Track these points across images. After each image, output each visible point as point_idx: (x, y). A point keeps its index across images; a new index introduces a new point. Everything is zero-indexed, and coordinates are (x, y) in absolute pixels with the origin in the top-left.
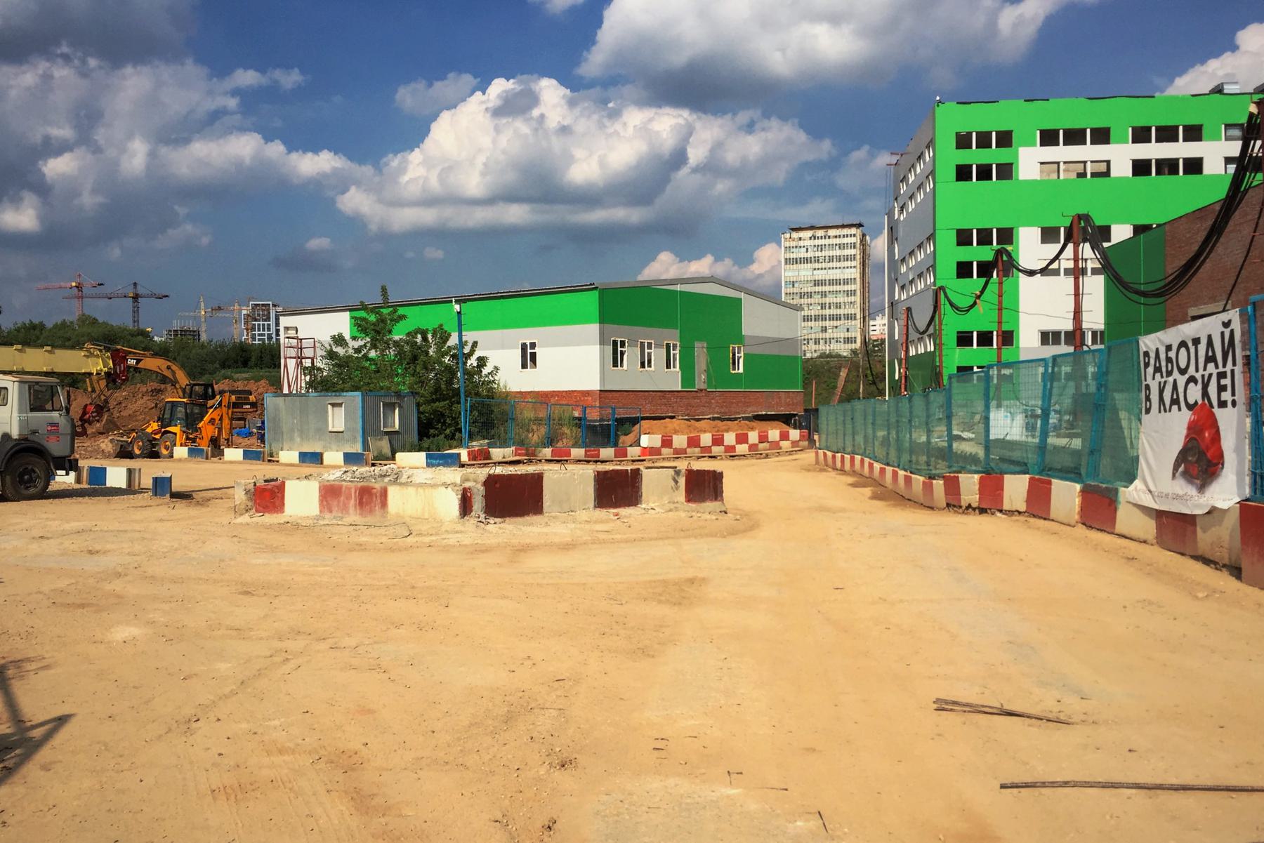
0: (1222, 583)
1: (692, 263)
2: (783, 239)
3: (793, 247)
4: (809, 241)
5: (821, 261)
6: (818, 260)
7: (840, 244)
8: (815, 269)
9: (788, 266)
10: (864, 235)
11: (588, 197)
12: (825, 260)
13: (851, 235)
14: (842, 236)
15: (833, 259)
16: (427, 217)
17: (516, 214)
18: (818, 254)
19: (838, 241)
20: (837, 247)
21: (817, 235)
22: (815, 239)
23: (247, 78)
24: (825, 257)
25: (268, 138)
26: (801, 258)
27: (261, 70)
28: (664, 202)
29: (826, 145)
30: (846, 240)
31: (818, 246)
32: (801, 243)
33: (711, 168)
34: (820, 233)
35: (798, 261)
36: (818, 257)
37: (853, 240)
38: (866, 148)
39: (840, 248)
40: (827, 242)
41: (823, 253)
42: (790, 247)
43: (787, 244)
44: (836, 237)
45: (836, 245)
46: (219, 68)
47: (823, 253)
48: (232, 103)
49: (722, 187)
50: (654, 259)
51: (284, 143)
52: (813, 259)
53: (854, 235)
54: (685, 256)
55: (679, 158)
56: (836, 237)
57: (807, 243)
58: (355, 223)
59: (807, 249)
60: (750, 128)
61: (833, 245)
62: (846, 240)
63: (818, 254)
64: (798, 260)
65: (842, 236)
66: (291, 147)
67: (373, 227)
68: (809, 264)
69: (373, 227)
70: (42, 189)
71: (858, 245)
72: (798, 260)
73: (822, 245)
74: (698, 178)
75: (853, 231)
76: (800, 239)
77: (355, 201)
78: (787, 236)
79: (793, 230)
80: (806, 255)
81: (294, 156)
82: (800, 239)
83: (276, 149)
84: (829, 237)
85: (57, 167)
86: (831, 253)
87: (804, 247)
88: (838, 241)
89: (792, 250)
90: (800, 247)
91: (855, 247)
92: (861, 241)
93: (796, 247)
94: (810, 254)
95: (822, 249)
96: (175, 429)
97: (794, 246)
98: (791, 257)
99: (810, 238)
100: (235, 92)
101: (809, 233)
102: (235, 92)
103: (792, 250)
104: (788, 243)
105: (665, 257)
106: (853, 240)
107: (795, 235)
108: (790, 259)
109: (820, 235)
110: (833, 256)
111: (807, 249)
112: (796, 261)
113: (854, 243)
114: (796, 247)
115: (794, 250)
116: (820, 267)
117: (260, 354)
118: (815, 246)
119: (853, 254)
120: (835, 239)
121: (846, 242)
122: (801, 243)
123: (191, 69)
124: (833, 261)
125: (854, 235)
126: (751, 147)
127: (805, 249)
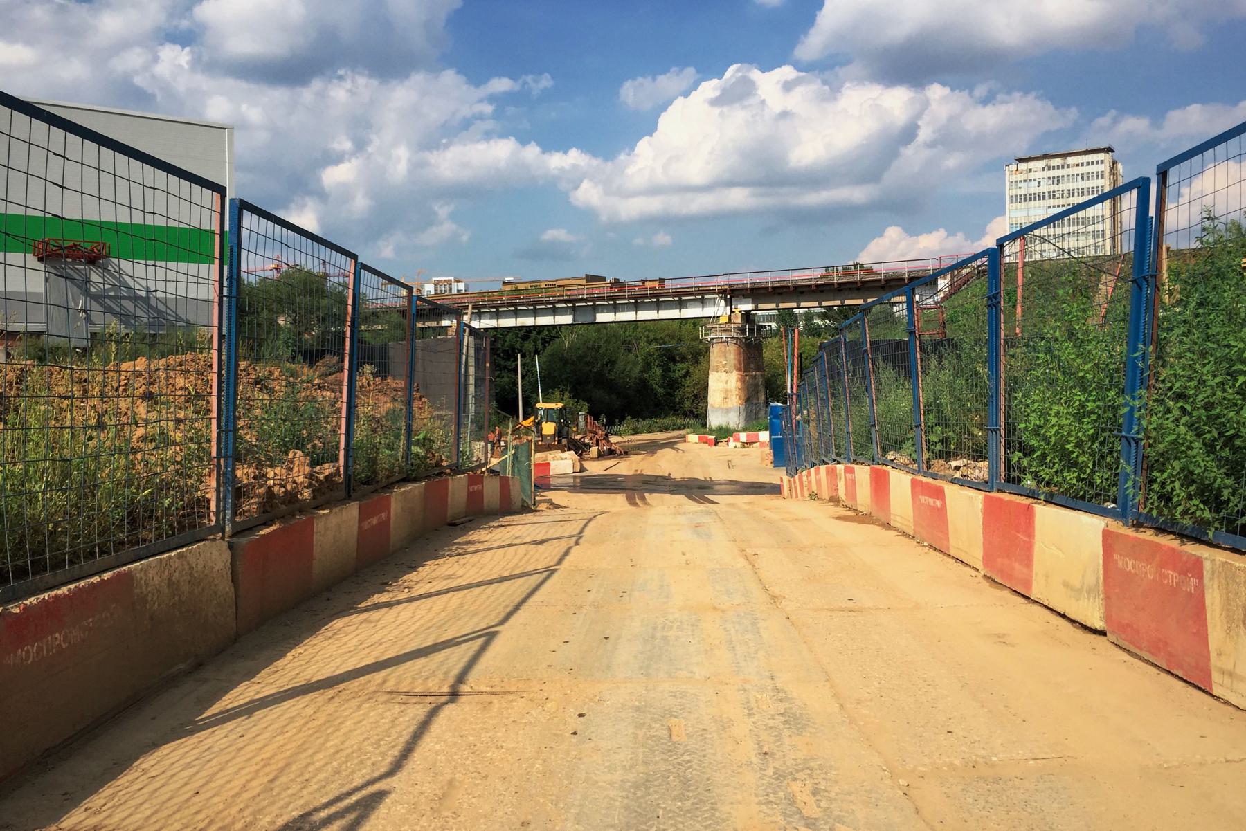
0: (553, 114)
1: (921, 238)
2: (1007, 172)
3: (1021, 181)
4: (1042, 172)
5: (1057, 196)
6: (1054, 196)
7: (1082, 174)
8: (1050, 207)
9: (1014, 205)
10: (1115, 163)
11: (813, 179)
12: (1063, 195)
13: (1097, 162)
14: (1085, 164)
15: (1073, 194)
16: (653, 205)
17: (738, 198)
18: (1055, 188)
19: (1080, 170)
20: (1079, 178)
21: (1052, 165)
22: (1049, 169)
23: (501, 85)
24: (1063, 191)
25: (524, 141)
26: (1031, 194)
27: (514, 78)
28: (889, 178)
29: (1073, 113)
30: (1090, 169)
31: (1054, 178)
32: (1032, 176)
33: (947, 139)
34: (1056, 162)
35: (1028, 198)
36: (1054, 192)
37: (1100, 168)
38: (1113, 112)
39: (1082, 178)
40: (1065, 172)
41: (1061, 187)
42: (1016, 182)
43: (1013, 178)
44: (1078, 165)
45: (1078, 175)
46: (476, 78)
47: (1061, 187)
48: (488, 109)
49: (952, 161)
50: (881, 234)
51: (539, 144)
52: (1047, 195)
53: (1102, 162)
54: (913, 231)
55: (908, 134)
56: (1078, 165)
57: (1041, 174)
58: (587, 215)
59: (1039, 183)
60: (987, 101)
61: (1073, 175)
62: (1090, 169)
63: (1055, 188)
64: (1028, 196)
65: (1085, 164)
66: (547, 148)
67: (604, 218)
68: (1042, 201)
69: (604, 218)
70: (322, 195)
71: (1107, 174)
72: (1028, 196)
73: (1058, 177)
74: (927, 153)
75: (1101, 156)
76: (1030, 171)
77: (588, 194)
78: (1013, 167)
79: (1021, 160)
80: (1037, 190)
81: (546, 157)
82: (1030, 171)
83: (532, 152)
84: (1068, 166)
85: (335, 176)
86: (1071, 186)
87: (1035, 180)
88: (1080, 170)
89: (1019, 185)
90: (1030, 180)
91: (1102, 177)
92: (1112, 169)
93: (1025, 181)
94: (1043, 189)
95: (1058, 181)
96: (661, 390)
97: (1022, 179)
98: (1019, 194)
99: (1044, 169)
100: (492, 99)
101: (1042, 163)
102: (492, 99)
103: (1019, 185)
104: (1014, 176)
105: (893, 232)
106: (1100, 168)
107: (1023, 166)
108: (1016, 196)
109: (1056, 164)
110: (1073, 190)
111: (1039, 183)
112: (1024, 198)
113: (1102, 172)
114: (1025, 181)
115: (1022, 185)
116: (1056, 204)
117: (683, 348)
118: (1049, 178)
119: (1100, 185)
120: (1076, 168)
121: (1090, 171)
122: (1032, 176)
123: (450, 77)
124: (1073, 196)
125: (1102, 162)
126: (989, 118)
127: (1036, 183)
